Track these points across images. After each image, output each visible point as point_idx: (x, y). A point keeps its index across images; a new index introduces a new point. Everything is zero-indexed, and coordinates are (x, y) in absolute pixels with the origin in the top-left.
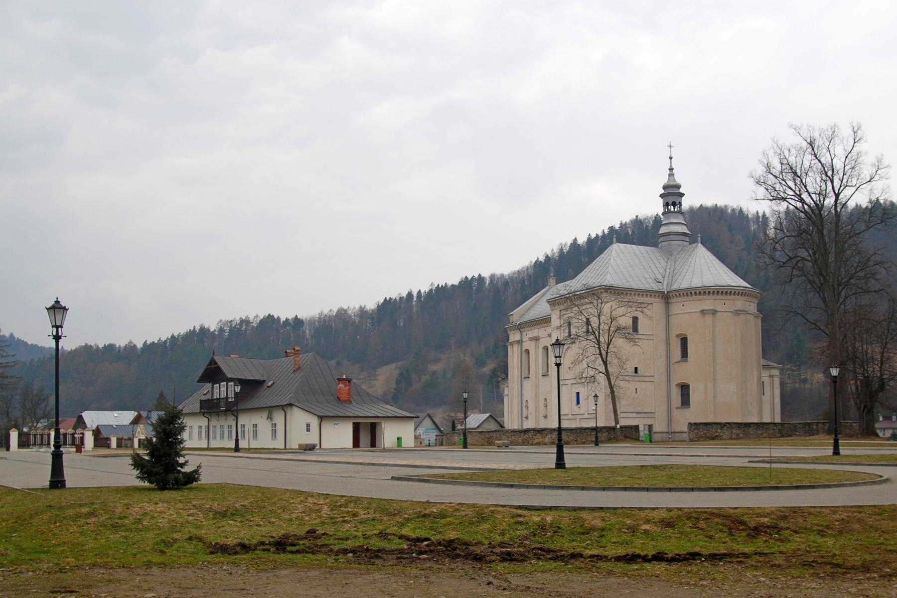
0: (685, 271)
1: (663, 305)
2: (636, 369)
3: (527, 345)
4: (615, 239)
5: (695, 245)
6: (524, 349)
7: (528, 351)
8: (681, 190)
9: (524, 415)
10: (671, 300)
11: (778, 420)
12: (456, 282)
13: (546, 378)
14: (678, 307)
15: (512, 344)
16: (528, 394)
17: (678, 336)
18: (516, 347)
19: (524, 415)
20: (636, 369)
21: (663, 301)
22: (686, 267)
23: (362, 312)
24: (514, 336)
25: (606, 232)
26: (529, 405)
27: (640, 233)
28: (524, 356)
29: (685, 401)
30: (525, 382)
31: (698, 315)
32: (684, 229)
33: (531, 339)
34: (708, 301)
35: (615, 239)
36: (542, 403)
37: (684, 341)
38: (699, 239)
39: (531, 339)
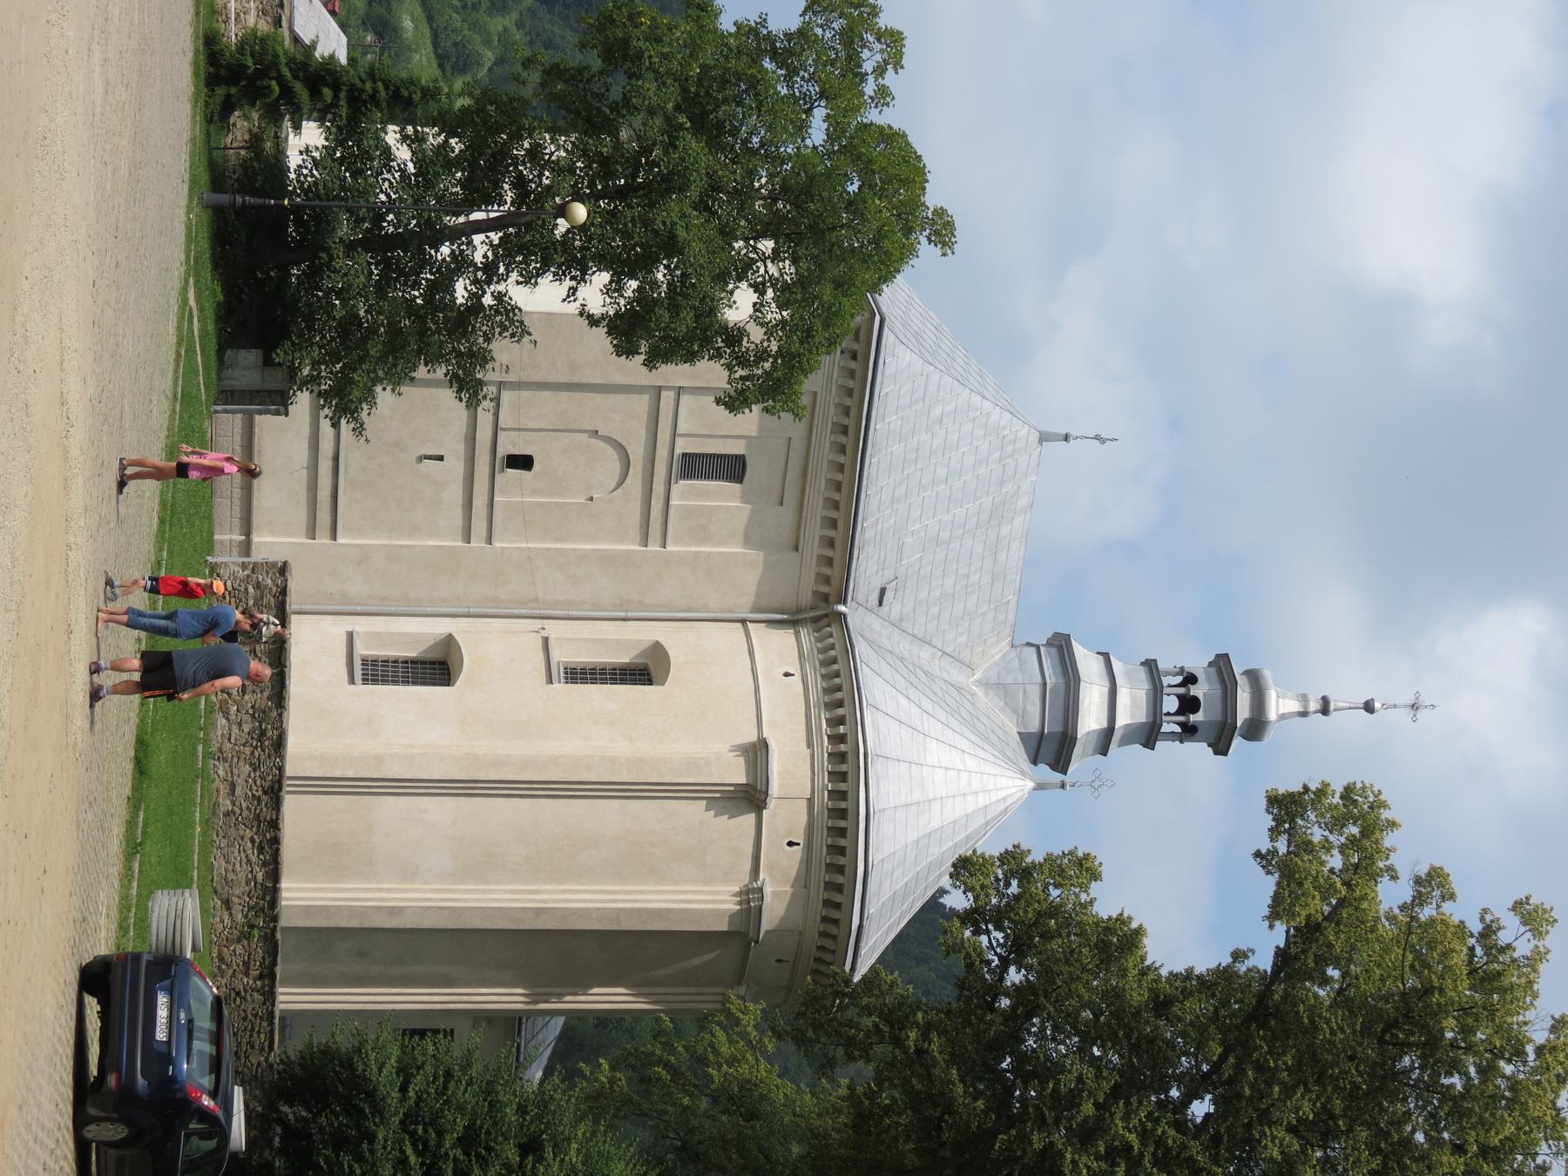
0: (927, 705)
2: (522, 462)
14: (780, 650)
20: (522, 462)
21: (806, 598)
37: (642, 672)
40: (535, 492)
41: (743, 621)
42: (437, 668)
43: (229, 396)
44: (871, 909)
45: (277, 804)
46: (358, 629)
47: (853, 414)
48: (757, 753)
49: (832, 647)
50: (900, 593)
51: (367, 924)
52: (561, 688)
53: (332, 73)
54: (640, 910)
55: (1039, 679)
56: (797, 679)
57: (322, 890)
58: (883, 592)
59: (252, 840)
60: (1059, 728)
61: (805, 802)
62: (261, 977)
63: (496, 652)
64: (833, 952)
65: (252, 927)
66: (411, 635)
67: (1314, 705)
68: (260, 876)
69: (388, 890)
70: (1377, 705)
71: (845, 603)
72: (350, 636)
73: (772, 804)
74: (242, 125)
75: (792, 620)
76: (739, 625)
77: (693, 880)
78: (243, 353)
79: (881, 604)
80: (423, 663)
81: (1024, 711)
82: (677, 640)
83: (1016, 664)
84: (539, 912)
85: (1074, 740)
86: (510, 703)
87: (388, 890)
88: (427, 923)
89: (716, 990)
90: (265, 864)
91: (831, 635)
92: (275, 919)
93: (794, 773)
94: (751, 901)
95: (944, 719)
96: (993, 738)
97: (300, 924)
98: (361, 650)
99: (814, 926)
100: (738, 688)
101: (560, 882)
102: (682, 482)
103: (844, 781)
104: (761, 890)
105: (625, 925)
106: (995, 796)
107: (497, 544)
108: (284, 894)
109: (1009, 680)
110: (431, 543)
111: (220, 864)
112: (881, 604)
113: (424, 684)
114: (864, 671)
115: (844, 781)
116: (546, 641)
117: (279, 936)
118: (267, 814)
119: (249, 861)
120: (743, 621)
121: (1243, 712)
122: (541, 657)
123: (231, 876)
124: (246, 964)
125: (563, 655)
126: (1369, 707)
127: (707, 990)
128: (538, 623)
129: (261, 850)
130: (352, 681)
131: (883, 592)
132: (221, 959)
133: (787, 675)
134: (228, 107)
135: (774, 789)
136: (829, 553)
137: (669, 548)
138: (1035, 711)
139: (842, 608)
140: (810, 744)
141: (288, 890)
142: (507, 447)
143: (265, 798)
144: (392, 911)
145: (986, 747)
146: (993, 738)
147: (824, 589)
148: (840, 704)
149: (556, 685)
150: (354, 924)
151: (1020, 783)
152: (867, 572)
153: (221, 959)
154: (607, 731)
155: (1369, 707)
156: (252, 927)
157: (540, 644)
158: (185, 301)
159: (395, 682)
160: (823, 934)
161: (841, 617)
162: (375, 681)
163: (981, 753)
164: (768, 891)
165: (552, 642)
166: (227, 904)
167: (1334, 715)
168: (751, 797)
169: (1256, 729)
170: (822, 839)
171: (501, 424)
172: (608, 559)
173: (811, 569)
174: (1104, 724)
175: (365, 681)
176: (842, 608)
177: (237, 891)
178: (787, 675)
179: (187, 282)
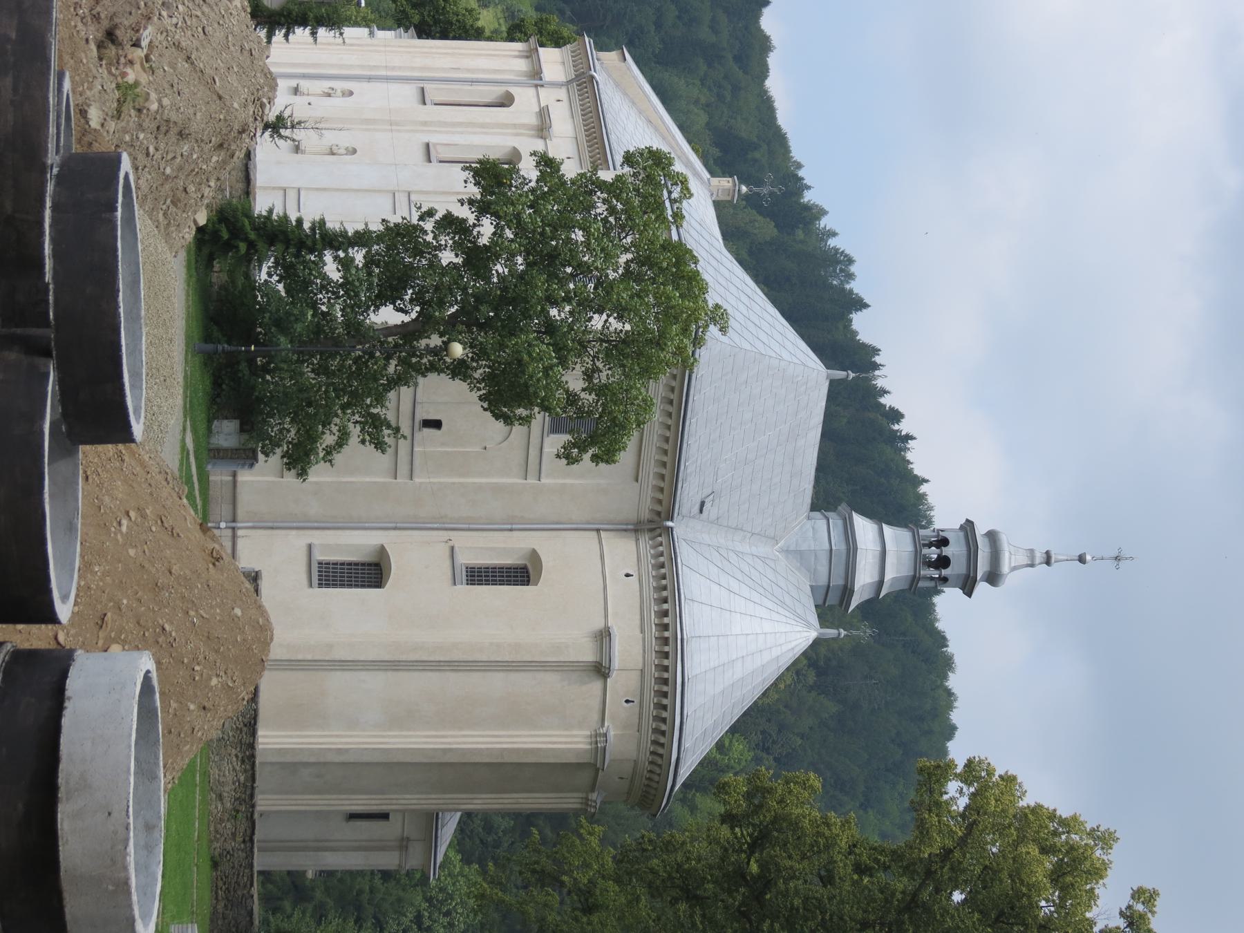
0: (734, 585)
1: (633, 517)
2: (437, 424)
3: (526, 99)
4: (840, 374)
5: (813, 618)
6: (514, 90)
7: (506, 101)
8: (982, 588)
9: (305, 85)
10: (645, 542)
11: (260, 862)
12: (940, 626)
13: (420, 154)
14: (624, 554)
15: (531, 55)
16: (371, 97)
17: (534, 556)
18: (522, 65)
19: (305, 85)
20: (437, 424)
21: (646, 515)
22: (745, 592)
23: (855, 333)
24: (554, 61)
25: (832, 242)
26: (337, 101)
27: (862, 461)
28: (496, 92)
29: (334, 575)
30: (409, 92)
31: (599, 624)
32: (865, 577)
33: (544, 114)
34: (637, 649)
35: (840, 374)
36: (343, 140)
37: (520, 575)
38: (831, 632)
39: (544, 114)
40: (443, 444)
41: (598, 530)
42: (371, 573)
43: (218, 455)
44: (687, 744)
45: (253, 734)
46: (316, 541)
47: (676, 391)
48: (604, 636)
49: (662, 554)
50: (717, 501)
51: (322, 760)
52: (464, 589)
53: (284, 233)
54: (518, 750)
55: (827, 546)
56: (634, 579)
57: (290, 737)
58: (702, 504)
59: (237, 756)
60: (841, 582)
61: (639, 673)
62: (244, 841)
63: (418, 561)
64: (660, 766)
65: (237, 811)
66: (353, 544)
67: (1039, 557)
68: (242, 779)
69: (337, 736)
70: (1088, 558)
71: (672, 520)
72: (310, 547)
73: (614, 675)
74: (219, 275)
75: (636, 529)
76: (595, 533)
77: (557, 730)
78: (225, 422)
79: (701, 511)
80: (363, 564)
81: (815, 570)
82: (550, 548)
83: (810, 534)
84: (445, 751)
85: (852, 591)
86: (426, 603)
87: (337, 736)
88: (366, 759)
89: (576, 795)
90: (245, 771)
91: (661, 544)
92: (253, 806)
93: (630, 650)
94: (599, 739)
95: (747, 595)
96: (788, 600)
97: (274, 760)
98: (319, 556)
99: (645, 757)
100: (590, 584)
101: (461, 729)
102: (552, 436)
103: (667, 658)
104: (605, 735)
105: (507, 759)
106: (785, 648)
107: (417, 480)
108: (260, 740)
109: (804, 547)
110: (368, 479)
111: (214, 772)
112: (701, 511)
113: (363, 586)
114: (684, 572)
115: (667, 658)
116: (452, 548)
117: (256, 816)
118: (246, 739)
119: (234, 769)
120: (598, 530)
121: (982, 568)
122: (448, 563)
123: (222, 779)
124: (234, 835)
125: (467, 558)
126: (1082, 559)
127: (569, 795)
128: (445, 535)
129: (243, 762)
130: (311, 586)
131: (702, 504)
132: (217, 832)
133: (627, 575)
134: (211, 259)
135: (616, 664)
136: (660, 496)
137: (543, 481)
138: (823, 569)
139: (670, 524)
140: (642, 631)
141: (264, 737)
142: (422, 414)
143: (245, 729)
144: (339, 751)
145: (781, 610)
146: (788, 600)
147: (659, 508)
148: (665, 601)
149: (459, 587)
150: (312, 760)
151: (806, 634)
152: (689, 493)
153: (217, 832)
154: (498, 617)
155: (1082, 559)
156: (237, 811)
157: (447, 553)
158: (183, 440)
159: (342, 586)
160: (655, 742)
161: (670, 530)
162: (328, 586)
163: (775, 616)
164: (612, 733)
165: (456, 549)
166: (220, 797)
167: (1055, 566)
168: (601, 670)
169: (993, 578)
170: (650, 699)
171: (419, 399)
172: (497, 489)
173: (649, 493)
174: (876, 578)
175: (320, 586)
176: (670, 524)
177: (227, 789)
178: (627, 575)
179: (184, 429)
